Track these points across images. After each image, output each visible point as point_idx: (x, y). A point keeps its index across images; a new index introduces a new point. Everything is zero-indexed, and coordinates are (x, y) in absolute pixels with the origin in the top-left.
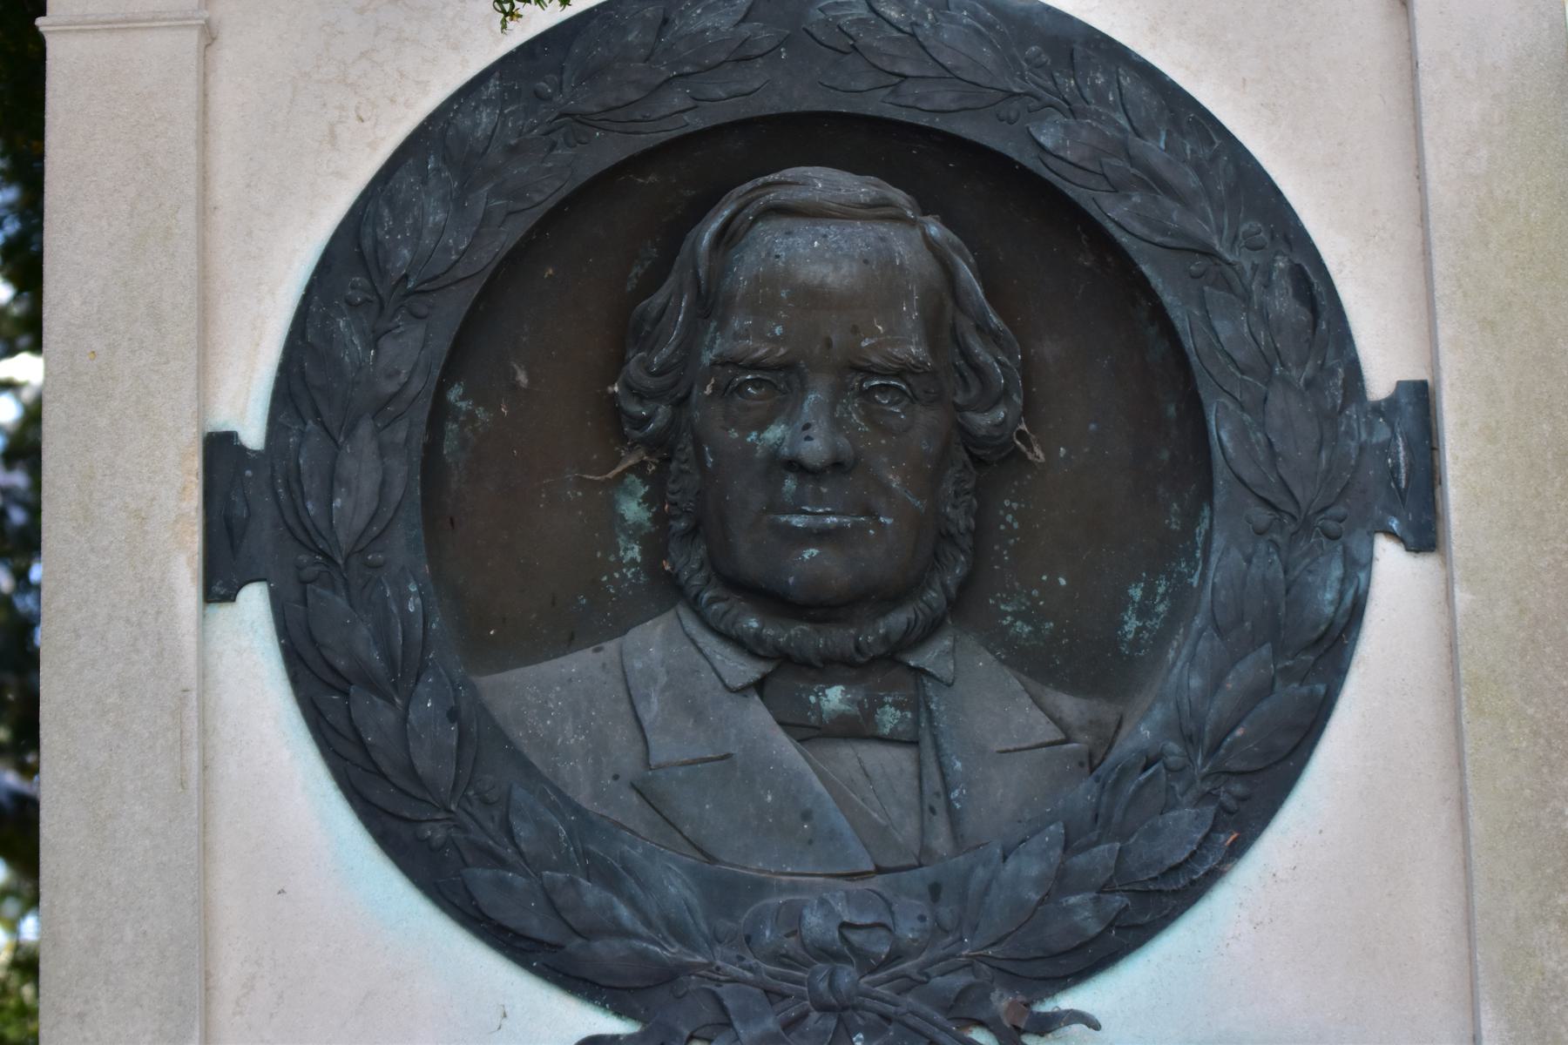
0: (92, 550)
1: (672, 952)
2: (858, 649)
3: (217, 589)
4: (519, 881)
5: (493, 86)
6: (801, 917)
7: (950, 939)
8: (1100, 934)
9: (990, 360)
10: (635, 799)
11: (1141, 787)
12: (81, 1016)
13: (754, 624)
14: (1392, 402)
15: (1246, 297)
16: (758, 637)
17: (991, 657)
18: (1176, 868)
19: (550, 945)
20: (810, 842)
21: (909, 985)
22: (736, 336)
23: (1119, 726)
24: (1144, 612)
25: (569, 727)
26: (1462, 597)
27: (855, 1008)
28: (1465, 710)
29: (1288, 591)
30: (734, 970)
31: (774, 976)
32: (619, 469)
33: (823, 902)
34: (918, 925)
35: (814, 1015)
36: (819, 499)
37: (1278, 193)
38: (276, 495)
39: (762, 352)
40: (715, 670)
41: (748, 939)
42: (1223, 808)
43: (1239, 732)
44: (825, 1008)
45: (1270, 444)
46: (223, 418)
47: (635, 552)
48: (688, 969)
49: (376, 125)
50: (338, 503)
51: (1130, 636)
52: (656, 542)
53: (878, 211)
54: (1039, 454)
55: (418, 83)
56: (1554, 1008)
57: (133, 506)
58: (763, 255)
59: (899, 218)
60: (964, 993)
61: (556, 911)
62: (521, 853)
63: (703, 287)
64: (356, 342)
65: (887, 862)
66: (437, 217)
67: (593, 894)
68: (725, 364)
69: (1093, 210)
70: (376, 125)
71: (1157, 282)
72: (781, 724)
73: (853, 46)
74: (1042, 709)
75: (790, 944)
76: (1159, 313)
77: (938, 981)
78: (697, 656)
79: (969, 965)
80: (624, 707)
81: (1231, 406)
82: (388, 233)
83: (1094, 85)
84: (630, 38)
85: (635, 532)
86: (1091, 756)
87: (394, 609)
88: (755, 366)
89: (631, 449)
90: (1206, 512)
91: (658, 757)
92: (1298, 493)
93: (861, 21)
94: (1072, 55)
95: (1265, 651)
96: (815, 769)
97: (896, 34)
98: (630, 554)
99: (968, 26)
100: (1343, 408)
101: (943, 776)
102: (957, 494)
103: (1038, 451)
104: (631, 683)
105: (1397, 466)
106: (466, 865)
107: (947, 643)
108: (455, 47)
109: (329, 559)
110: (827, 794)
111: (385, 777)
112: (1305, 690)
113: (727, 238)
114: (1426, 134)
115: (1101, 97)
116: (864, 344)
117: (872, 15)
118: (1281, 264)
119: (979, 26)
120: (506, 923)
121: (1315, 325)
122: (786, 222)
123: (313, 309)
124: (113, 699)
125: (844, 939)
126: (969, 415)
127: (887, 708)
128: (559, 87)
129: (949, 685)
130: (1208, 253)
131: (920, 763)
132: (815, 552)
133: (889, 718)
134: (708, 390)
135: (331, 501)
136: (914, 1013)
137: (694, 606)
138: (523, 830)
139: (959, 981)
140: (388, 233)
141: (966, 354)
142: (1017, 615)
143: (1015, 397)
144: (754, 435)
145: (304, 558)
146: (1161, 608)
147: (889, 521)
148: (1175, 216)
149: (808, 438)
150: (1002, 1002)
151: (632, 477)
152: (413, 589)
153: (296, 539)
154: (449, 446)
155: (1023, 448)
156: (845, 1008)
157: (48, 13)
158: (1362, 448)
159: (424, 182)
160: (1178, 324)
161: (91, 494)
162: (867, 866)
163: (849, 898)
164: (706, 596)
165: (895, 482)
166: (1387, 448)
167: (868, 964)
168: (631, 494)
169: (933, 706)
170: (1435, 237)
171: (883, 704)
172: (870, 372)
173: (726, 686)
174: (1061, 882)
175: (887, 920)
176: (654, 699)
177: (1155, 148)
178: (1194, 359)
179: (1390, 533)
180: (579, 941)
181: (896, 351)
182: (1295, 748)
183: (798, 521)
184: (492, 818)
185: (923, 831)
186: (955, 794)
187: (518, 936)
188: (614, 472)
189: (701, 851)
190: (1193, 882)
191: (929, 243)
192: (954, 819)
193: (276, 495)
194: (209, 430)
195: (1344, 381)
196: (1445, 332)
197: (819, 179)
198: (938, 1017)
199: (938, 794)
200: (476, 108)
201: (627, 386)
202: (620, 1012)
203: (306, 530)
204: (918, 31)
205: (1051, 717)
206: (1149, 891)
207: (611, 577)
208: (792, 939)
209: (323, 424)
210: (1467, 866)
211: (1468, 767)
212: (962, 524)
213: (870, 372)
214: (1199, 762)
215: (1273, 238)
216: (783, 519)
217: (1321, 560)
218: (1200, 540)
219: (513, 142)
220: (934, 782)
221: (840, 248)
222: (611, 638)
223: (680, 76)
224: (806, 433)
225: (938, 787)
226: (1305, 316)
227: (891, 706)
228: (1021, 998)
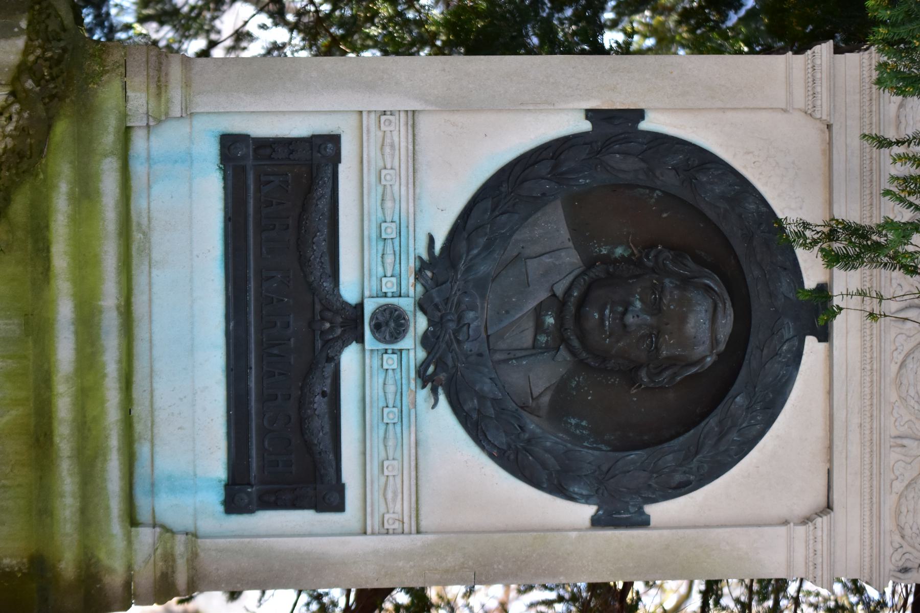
0: (603, 73)
1: (462, 267)
2: (566, 329)
3: (590, 113)
4: (486, 217)
5: (763, 209)
6: (472, 310)
7: (464, 360)
8: (464, 410)
9: (664, 377)
10: (515, 254)
11: (513, 425)
12: (444, 70)
13: (575, 294)
14: (643, 513)
15: (681, 465)
16: (571, 295)
17: (564, 373)
18: (485, 436)
19: (465, 227)
20: (498, 313)
21: (449, 345)
22: (671, 292)
23: (538, 416)
24: (577, 426)
25: (541, 231)
26: (574, 534)
27: (442, 327)
28: (535, 534)
29: (578, 476)
30: (455, 288)
31: (453, 300)
32: (633, 247)
33: (477, 318)
34: (469, 349)
35: (439, 314)
36: (614, 319)
37: (717, 477)
38: (622, 134)
39: (665, 301)
40: (560, 280)
41: (465, 292)
42: (505, 452)
43: (530, 458)
44: (442, 318)
45: (629, 472)
46: (649, 116)
47: (604, 252)
48: (456, 272)
49: (752, 168)
50: (618, 156)
51: (569, 421)
52: (607, 260)
53: (715, 342)
54: (634, 391)
55: (767, 182)
56: (435, 559)
57: (618, 86)
58: (699, 302)
59: (713, 348)
60: (446, 364)
61: (477, 229)
62: (496, 217)
63: (692, 280)
64: (675, 162)
65: (491, 339)
66: (717, 190)
67: (482, 241)
68: (662, 288)
69: (713, 414)
70: (752, 168)
71: (687, 435)
72: (542, 302)
73: (774, 333)
74: (545, 390)
75: (463, 307)
76: (678, 435)
77: (450, 355)
78: (565, 274)
79: (455, 366)
80: (548, 250)
81: (643, 459)
82: (712, 173)
83: (758, 416)
84: (779, 257)
85: (611, 252)
86: (527, 407)
87: (581, 175)
88: (661, 299)
89: (640, 252)
90: (609, 449)
91: (529, 262)
92: (612, 480)
93: (782, 336)
94: (768, 408)
95: (558, 468)
96: (523, 316)
97: (778, 348)
98: (603, 250)
99: (779, 373)
100: (642, 497)
101: (521, 357)
102: (619, 364)
103: (635, 391)
104: (556, 252)
105: (620, 514)
106: (493, 198)
107: (568, 359)
108: (779, 196)
109: (599, 152)
110: (514, 319)
111: (524, 171)
112: (544, 480)
113: (708, 289)
114: (735, 529)
115: (752, 418)
116: (666, 336)
117: (785, 340)
118: (692, 477)
119: (779, 377)
120: (473, 212)
121: (670, 488)
122: (711, 310)
123: (686, 147)
124: (551, 80)
125: (465, 325)
126: (646, 369)
127: (546, 338)
128: (763, 232)
129: (553, 359)
130: (697, 453)
131: (526, 349)
132: (597, 317)
133: (543, 339)
134: (655, 281)
135: (618, 153)
136: (439, 348)
137: (583, 273)
138: (504, 217)
139: (450, 363)
140: (712, 173)
141: (666, 369)
142: (578, 382)
143: (652, 384)
144: (638, 297)
145: (599, 144)
146: (578, 432)
147: (607, 342)
148: (710, 442)
149: (633, 317)
150: (443, 376)
151: (631, 252)
152: (587, 181)
153: (607, 141)
154: (641, 190)
155: (635, 386)
156: (442, 324)
157: (794, 56)
158: (627, 502)
159: (730, 185)
160: (672, 442)
161: (623, 72)
162: (490, 332)
163: (478, 326)
164: (586, 278)
165: (620, 344)
166: (627, 511)
167: (456, 332)
168: (625, 251)
169: (545, 354)
170: (698, 530)
171: (548, 336)
172: (657, 338)
173: (554, 284)
174: (482, 397)
175: (471, 339)
176: (550, 260)
177: (734, 436)
178: (660, 447)
179: (598, 511)
180: (466, 236)
181: (664, 347)
182: (525, 476)
183: (607, 312)
184: (508, 207)
185: (502, 350)
186: (514, 361)
187: (468, 216)
188: (632, 245)
189: (496, 277)
190: (481, 441)
191: (704, 358)
192: (506, 361)
193: (622, 134)
194: (646, 111)
195: (651, 498)
196: (666, 532)
197: (727, 320)
198: (438, 355)
199: (515, 355)
200: (756, 203)
201: (660, 251)
202: (443, 249)
203: (609, 144)
204: (778, 356)
205: (542, 393)
206: (478, 426)
207: (595, 244)
208: (465, 307)
209: (646, 150)
210: (484, 532)
211: (516, 534)
212: (608, 365)
213: (657, 338)
214: (521, 444)
215: (702, 475)
216: (609, 307)
217: (589, 488)
218: (600, 446)
219: (743, 216)
220: (519, 354)
221: (700, 329)
222: (573, 243)
223: (765, 274)
224: (636, 316)
225: (517, 356)
226: (673, 485)
227: (547, 339)
228: (444, 382)
